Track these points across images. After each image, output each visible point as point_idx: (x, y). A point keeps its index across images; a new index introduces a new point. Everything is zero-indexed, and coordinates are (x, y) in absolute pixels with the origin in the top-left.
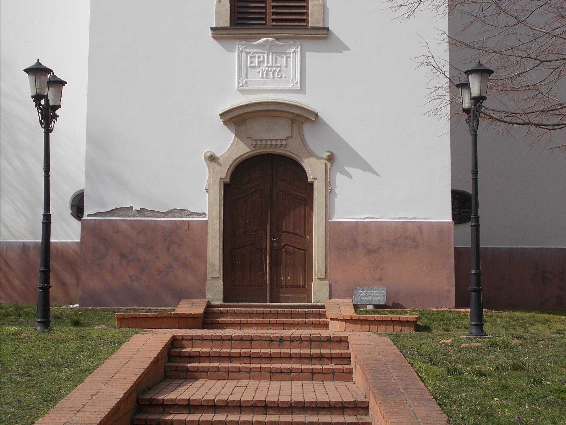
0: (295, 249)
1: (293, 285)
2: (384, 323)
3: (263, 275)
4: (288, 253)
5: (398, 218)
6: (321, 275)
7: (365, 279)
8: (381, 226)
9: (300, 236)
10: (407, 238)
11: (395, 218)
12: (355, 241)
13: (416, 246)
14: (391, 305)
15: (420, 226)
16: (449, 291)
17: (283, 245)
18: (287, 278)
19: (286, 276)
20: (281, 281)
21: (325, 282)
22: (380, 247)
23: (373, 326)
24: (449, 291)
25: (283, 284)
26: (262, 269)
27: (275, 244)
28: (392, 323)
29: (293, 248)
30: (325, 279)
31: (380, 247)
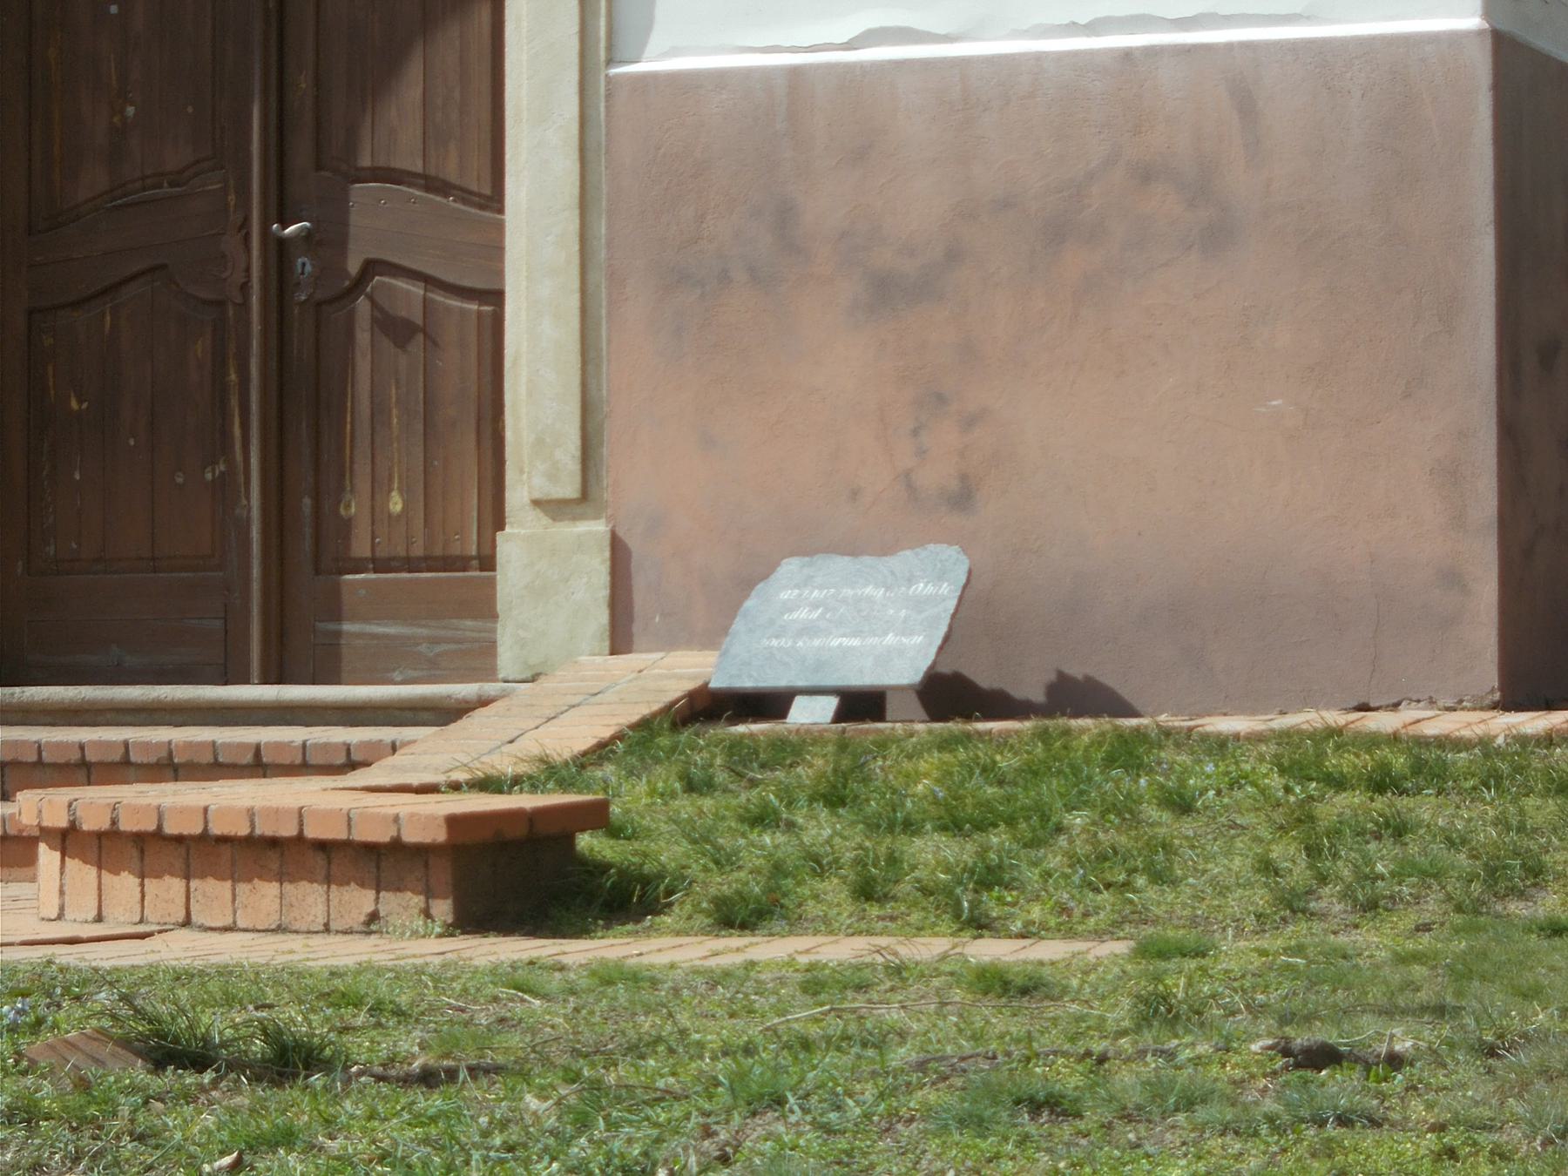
0: (438, 297)
1: (418, 551)
2: (273, 860)
3: (226, 490)
4: (396, 330)
5: (1093, 28)
6: (552, 477)
7: (855, 494)
8: (971, 99)
9: (465, 195)
10: (1145, 175)
11: (1073, 28)
12: (784, 216)
13: (1217, 237)
14: (1038, 696)
15: (1240, 79)
16: (1453, 579)
17: (354, 266)
18: (377, 504)
19: (378, 489)
20: (346, 526)
21: (583, 527)
22: (954, 256)
23: (211, 881)
24: (1453, 579)
25: (361, 547)
26: (225, 448)
27: (304, 265)
28: (319, 860)
29: (417, 290)
30: (586, 499)
31: (954, 256)
